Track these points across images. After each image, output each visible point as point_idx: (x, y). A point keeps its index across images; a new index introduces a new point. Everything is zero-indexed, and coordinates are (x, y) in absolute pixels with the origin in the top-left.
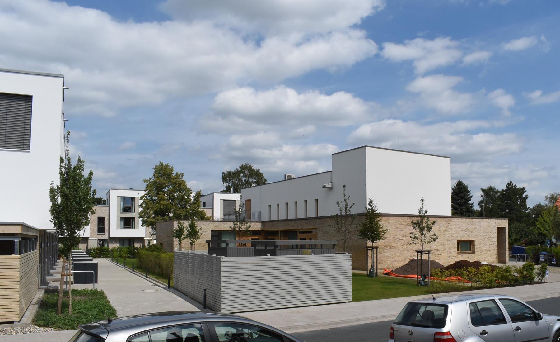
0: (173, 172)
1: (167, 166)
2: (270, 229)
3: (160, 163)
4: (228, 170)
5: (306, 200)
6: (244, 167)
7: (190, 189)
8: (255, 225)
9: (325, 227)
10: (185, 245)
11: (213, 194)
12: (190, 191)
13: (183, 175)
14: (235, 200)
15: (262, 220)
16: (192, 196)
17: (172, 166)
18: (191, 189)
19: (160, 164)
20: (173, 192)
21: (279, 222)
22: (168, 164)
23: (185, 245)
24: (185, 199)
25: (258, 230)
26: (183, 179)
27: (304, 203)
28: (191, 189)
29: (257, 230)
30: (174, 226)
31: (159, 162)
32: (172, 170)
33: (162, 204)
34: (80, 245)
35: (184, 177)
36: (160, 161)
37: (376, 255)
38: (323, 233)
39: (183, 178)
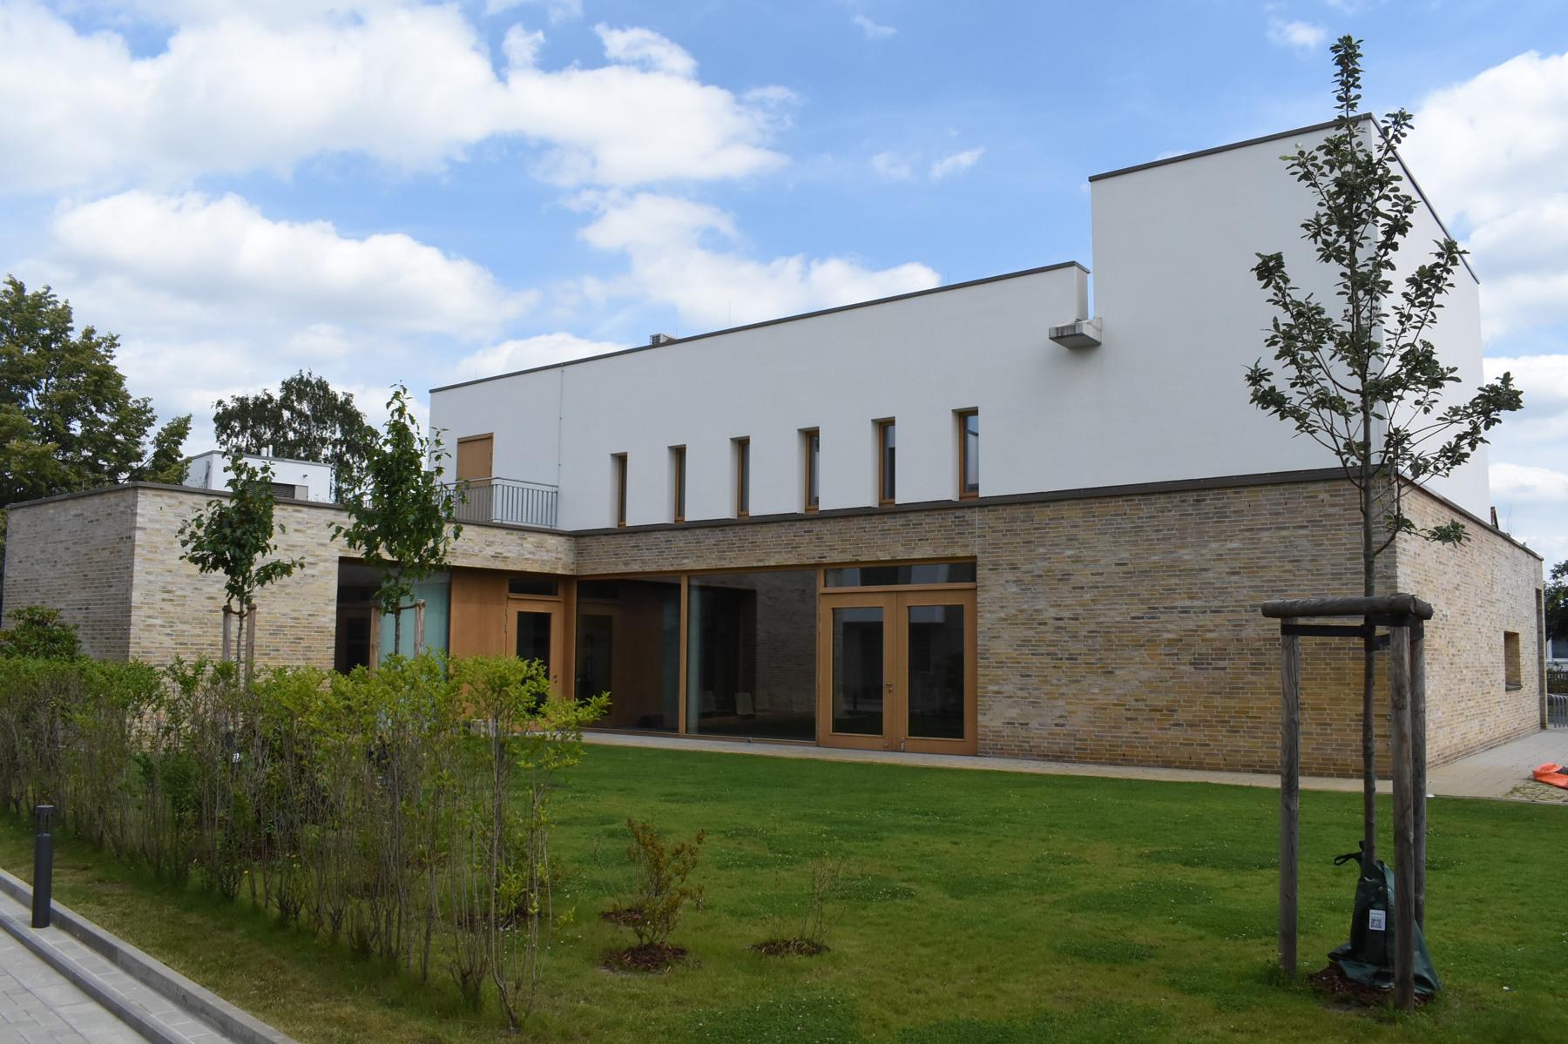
0: (69, 325)
1: (39, 300)
2: (622, 569)
3: (12, 283)
4: (240, 395)
5: (809, 424)
6: (297, 388)
7: (145, 406)
8: (539, 546)
9: (1042, 550)
10: (198, 631)
11: (208, 457)
12: (145, 412)
13: (112, 342)
14: (293, 487)
15: (569, 523)
16: (152, 438)
17: (67, 302)
18: (150, 405)
19: (10, 288)
20: (68, 410)
21: (686, 533)
22: (49, 288)
23: (198, 631)
24: (115, 443)
25: (553, 571)
26: (112, 363)
27: (794, 449)
28: (150, 405)
29: (546, 570)
30: (139, 519)
31: (8, 279)
32: (64, 315)
33: (17, 454)
34: (133, 836)
35: (115, 351)
36: (10, 276)
37: (1376, 710)
38: (1018, 582)
39: (112, 357)
